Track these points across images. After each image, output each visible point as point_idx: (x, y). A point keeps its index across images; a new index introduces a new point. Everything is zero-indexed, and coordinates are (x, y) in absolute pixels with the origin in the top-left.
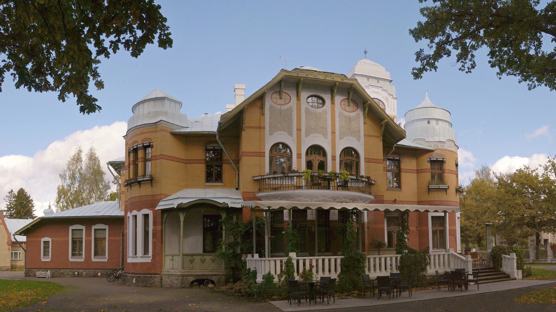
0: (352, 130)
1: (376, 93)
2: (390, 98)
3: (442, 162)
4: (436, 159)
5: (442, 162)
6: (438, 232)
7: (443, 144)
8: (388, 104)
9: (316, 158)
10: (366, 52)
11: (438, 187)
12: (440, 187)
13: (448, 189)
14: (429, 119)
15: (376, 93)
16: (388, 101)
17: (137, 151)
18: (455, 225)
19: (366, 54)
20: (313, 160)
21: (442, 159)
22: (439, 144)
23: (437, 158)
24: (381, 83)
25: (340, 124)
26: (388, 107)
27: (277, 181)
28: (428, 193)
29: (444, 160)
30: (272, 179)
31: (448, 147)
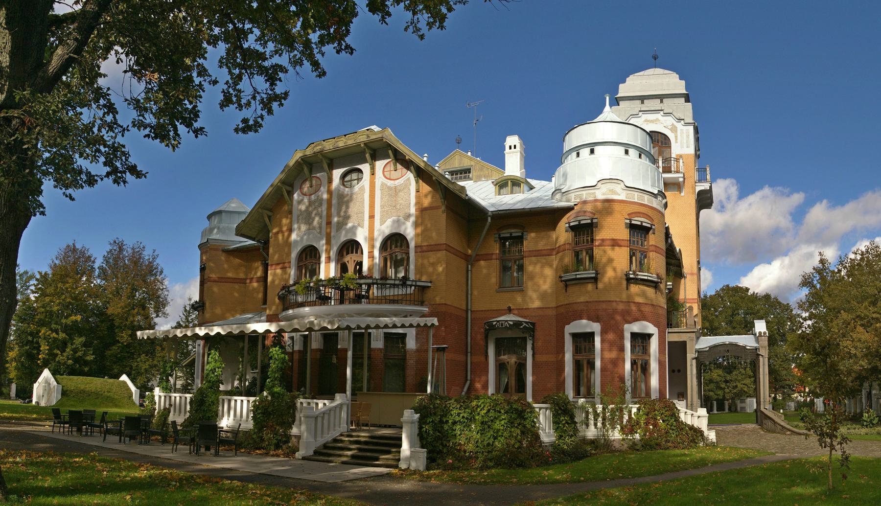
0: (398, 207)
1: (652, 121)
2: (679, 126)
4: (639, 223)
7: (593, 191)
8: (676, 137)
9: (351, 258)
10: (655, 58)
11: (575, 277)
12: (578, 276)
14: (577, 149)
15: (652, 121)
16: (677, 132)
19: (655, 59)
20: (348, 262)
21: (589, 221)
22: (584, 193)
23: (642, 222)
24: (668, 103)
25: (381, 202)
28: (564, 291)
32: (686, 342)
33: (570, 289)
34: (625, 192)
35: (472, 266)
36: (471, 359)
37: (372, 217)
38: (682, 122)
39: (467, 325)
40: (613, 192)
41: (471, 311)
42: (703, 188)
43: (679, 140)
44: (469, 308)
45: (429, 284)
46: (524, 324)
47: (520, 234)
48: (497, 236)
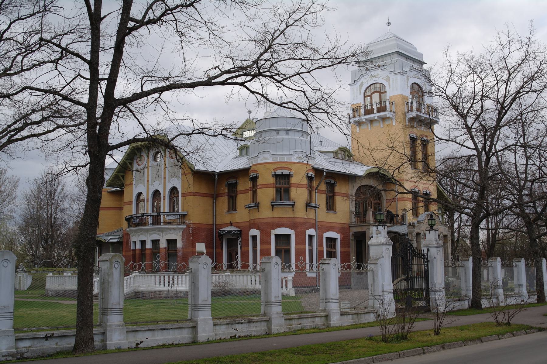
3: (288, 177)
4: (281, 173)
5: (288, 177)
6: (283, 251)
8: (389, 84)
13: (294, 205)
17: (236, 197)
18: (341, 252)
21: (288, 173)
23: (282, 173)
26: (390, 88)
27: (170, 217)
29: (291, 173)
30: (172, 216)
31: (261, 160)
32: (176, 240)
33: (275, 210)
34: (272, 157)
35: (215, 200)
36: (216, 250)
37: (165, 178)
38: (392, 73)
39: (213, 232)
40: (266, 158)
41: (216, 225)
42: (411, 116)
43: (391, 87)
44: (214, 223)
45: (186, 213)
46: (233, 232)
47: (235, 182)
48: (226, 183)
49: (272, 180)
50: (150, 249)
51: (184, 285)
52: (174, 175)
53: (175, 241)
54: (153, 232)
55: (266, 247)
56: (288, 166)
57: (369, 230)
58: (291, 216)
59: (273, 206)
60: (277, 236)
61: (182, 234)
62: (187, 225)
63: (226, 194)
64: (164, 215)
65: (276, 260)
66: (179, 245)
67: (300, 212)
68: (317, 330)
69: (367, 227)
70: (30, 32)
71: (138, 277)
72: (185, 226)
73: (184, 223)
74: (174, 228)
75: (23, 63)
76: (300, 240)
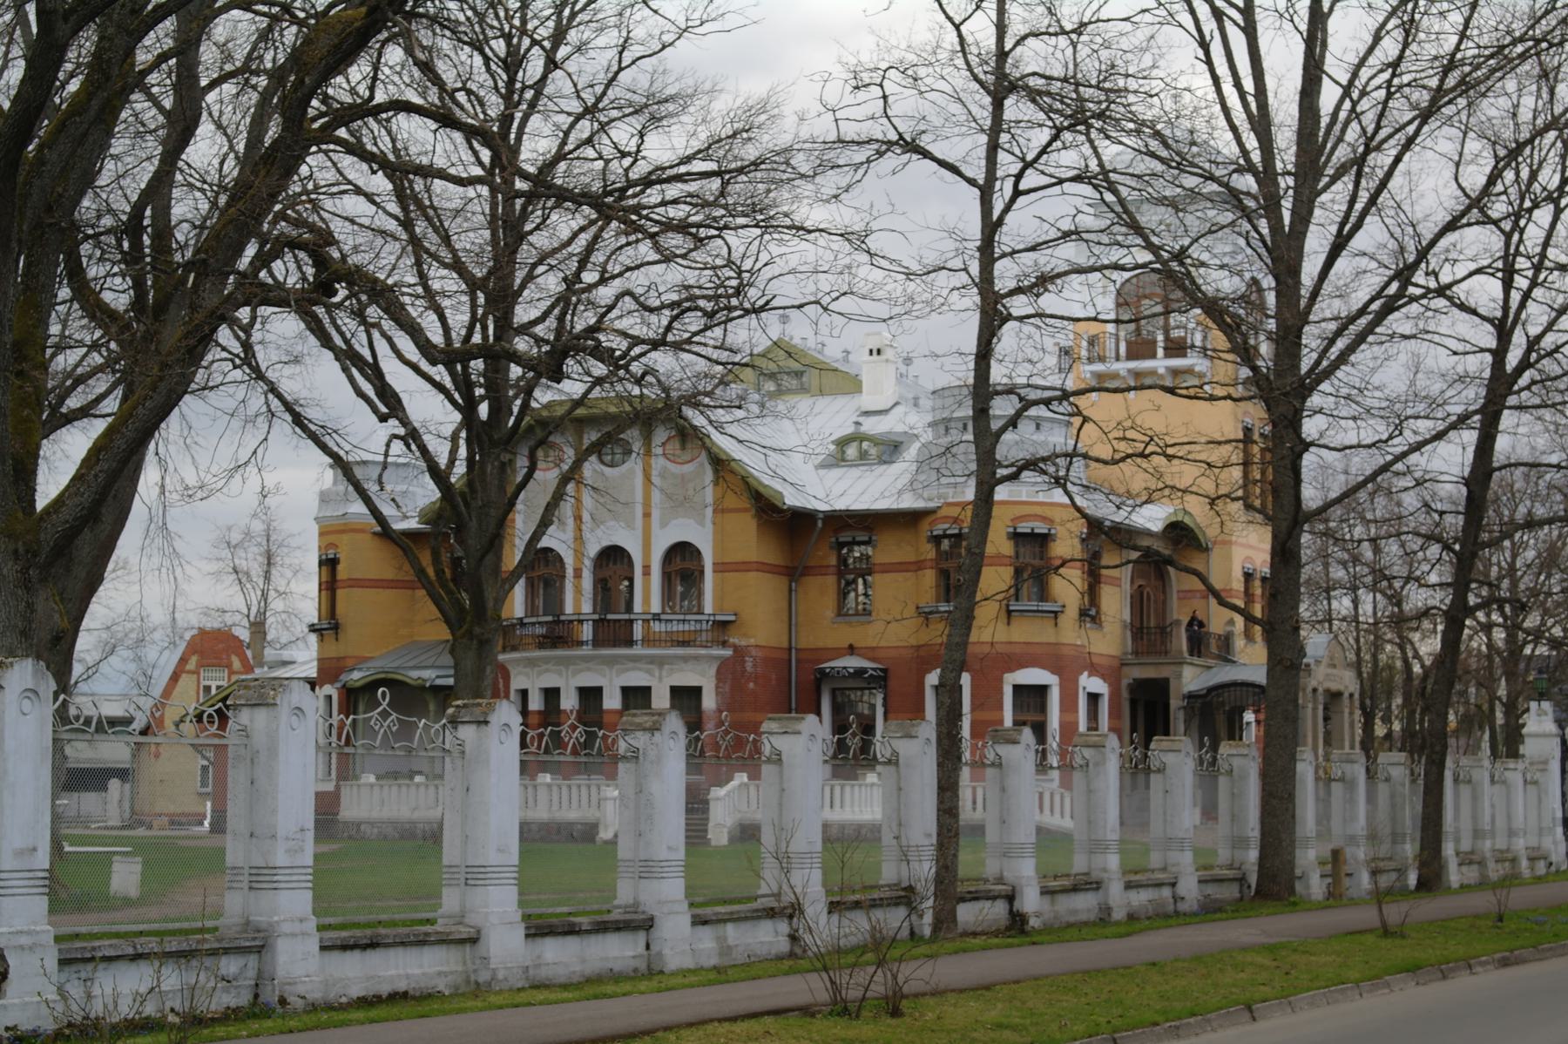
3: (1043, 540)
5: (1043, 540)
32: (649, 688)
33: (1015, 623)
37: (647, 515)
45: (732, 618)
49: (1007, 548)
50: (539, 712)
51: (847, 808)
52: (680, 503)
53: (697, 691)
54: (631, 665)
55: (986, 715)
56: (1048, 512)
57: (1179, 676)
58: (1052, 640)
59: (1009, 612)
60: (1018, 689)
61: (718, 672)
62: (736, 648)
63: (833, 570)
64: (646, 621)
65: (1021, 753)
66: (709, 702)
67: (1070, 633)
68: (712, 976)
69: (1173, 668)
70: (1427, 417)
71: (422, 789)
72: (728, 652)
73: (724, 644)
74: (696, 658)
75: (628, 274)
76: (1068, 704)
